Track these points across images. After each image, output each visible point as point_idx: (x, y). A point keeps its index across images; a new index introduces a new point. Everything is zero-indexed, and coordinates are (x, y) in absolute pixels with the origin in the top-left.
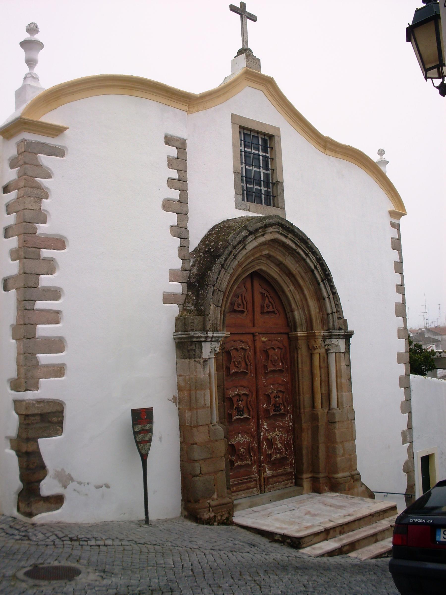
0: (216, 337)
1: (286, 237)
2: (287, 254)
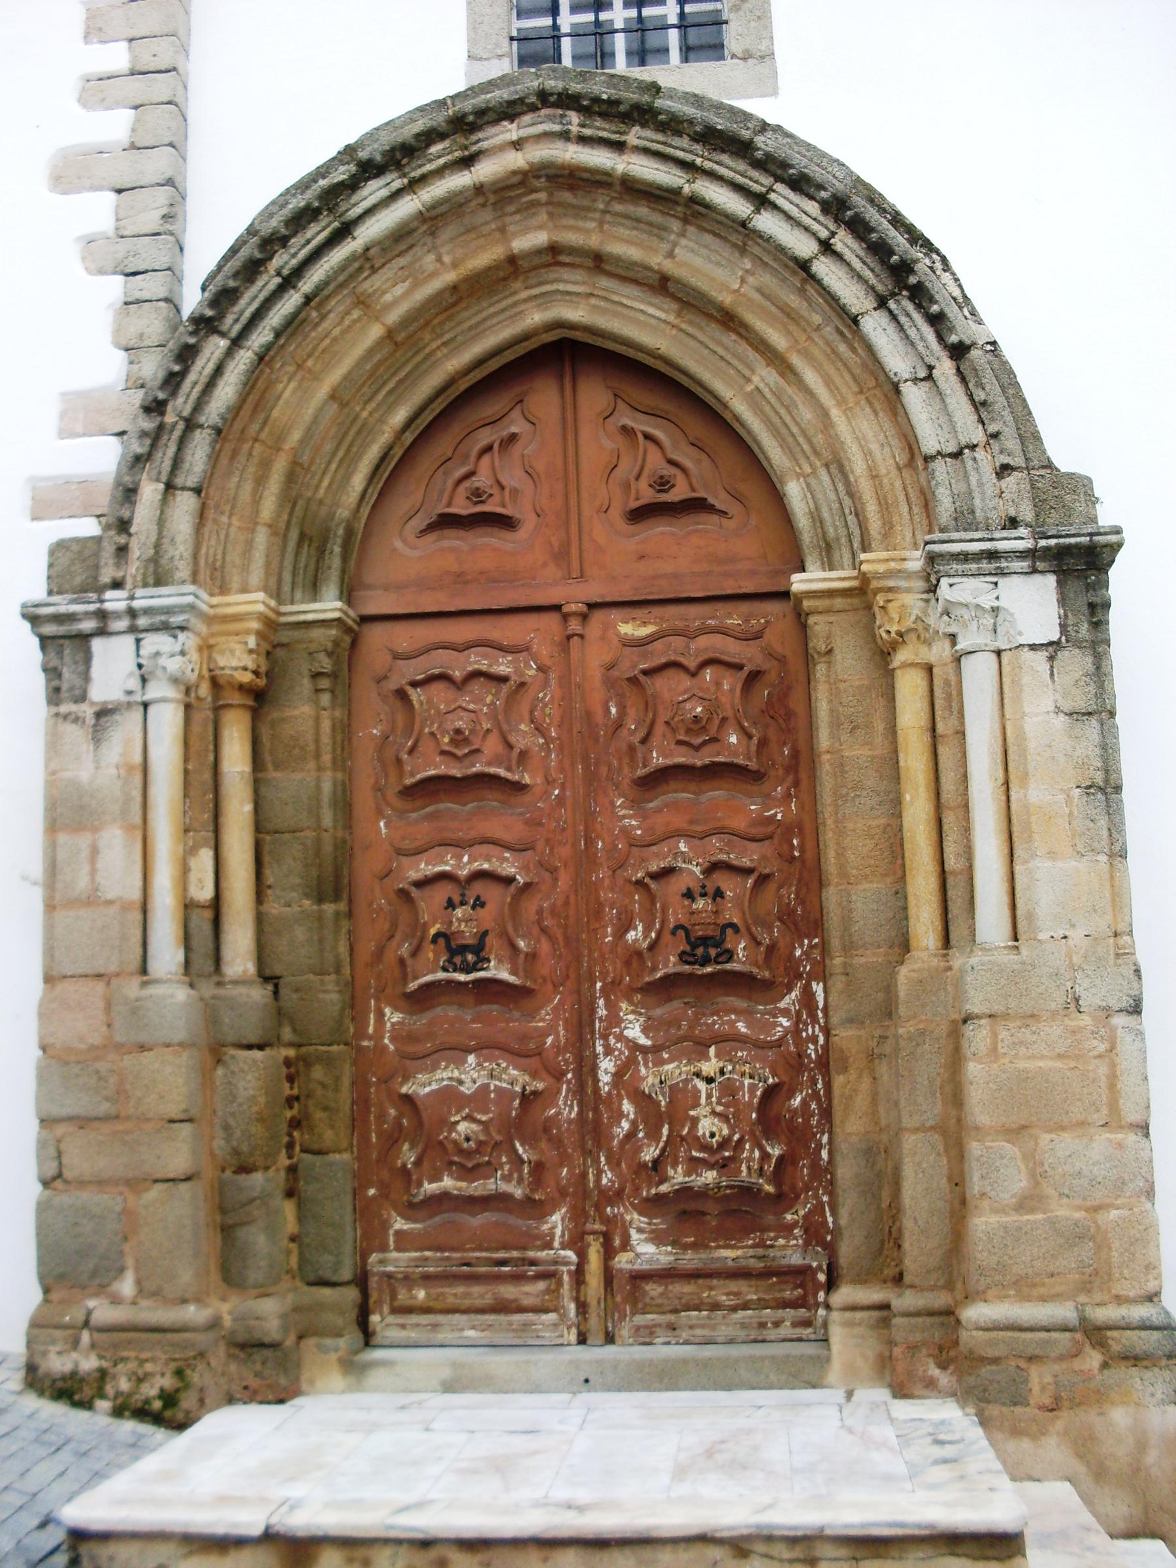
0: (148, 611)
1: (619, 147)
2: (676, 225)
